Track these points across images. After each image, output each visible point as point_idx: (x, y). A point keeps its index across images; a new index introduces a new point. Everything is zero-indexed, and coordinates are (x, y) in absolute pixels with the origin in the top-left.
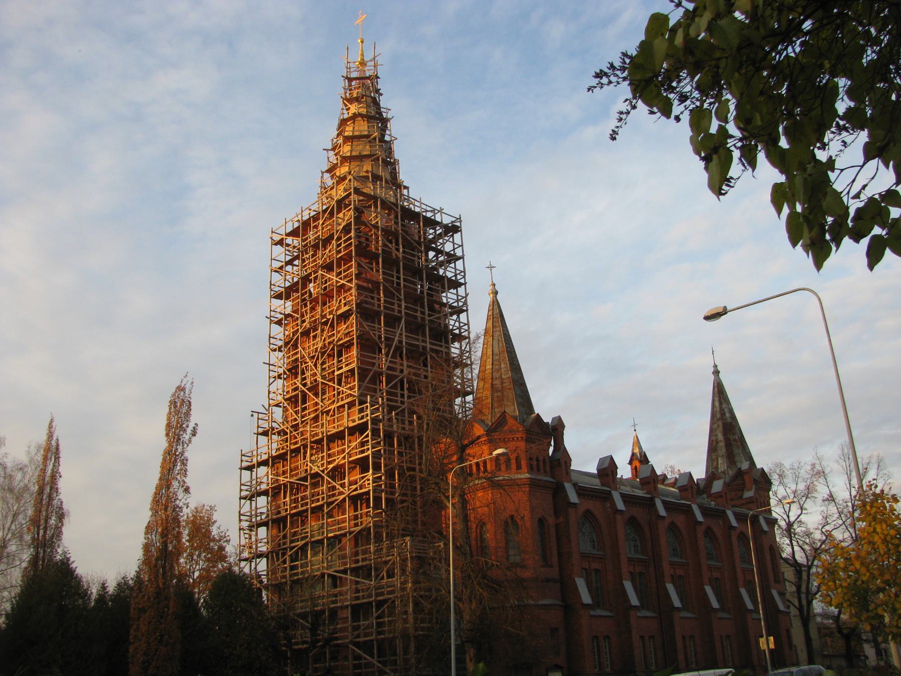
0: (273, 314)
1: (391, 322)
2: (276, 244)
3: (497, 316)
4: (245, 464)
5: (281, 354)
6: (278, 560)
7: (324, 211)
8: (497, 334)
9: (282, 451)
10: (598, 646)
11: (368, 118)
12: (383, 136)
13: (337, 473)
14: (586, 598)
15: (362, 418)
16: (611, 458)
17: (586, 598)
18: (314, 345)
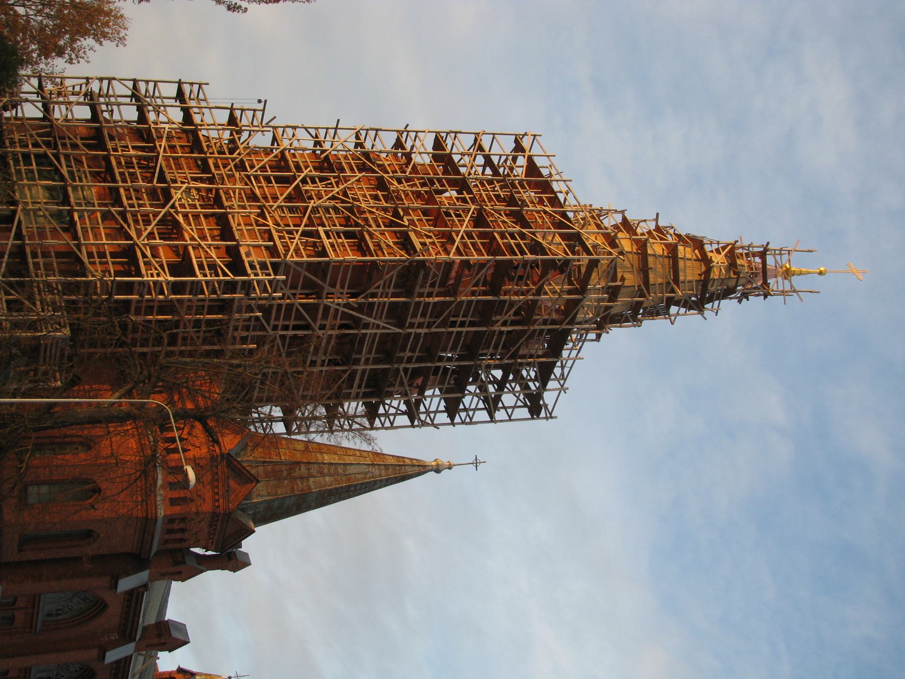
0: (413, 135)
1: (397, 314)
2: (516, 141)
3: (402, 471)
4: (186, 88)
5: (351, 146)
7: (564, 215)
8: (376, 471)
9: (204, 145)
11: (705, 281)
12: (677, 304)
13: (171, 228)
15: (252, 267)
16: (185, 642)
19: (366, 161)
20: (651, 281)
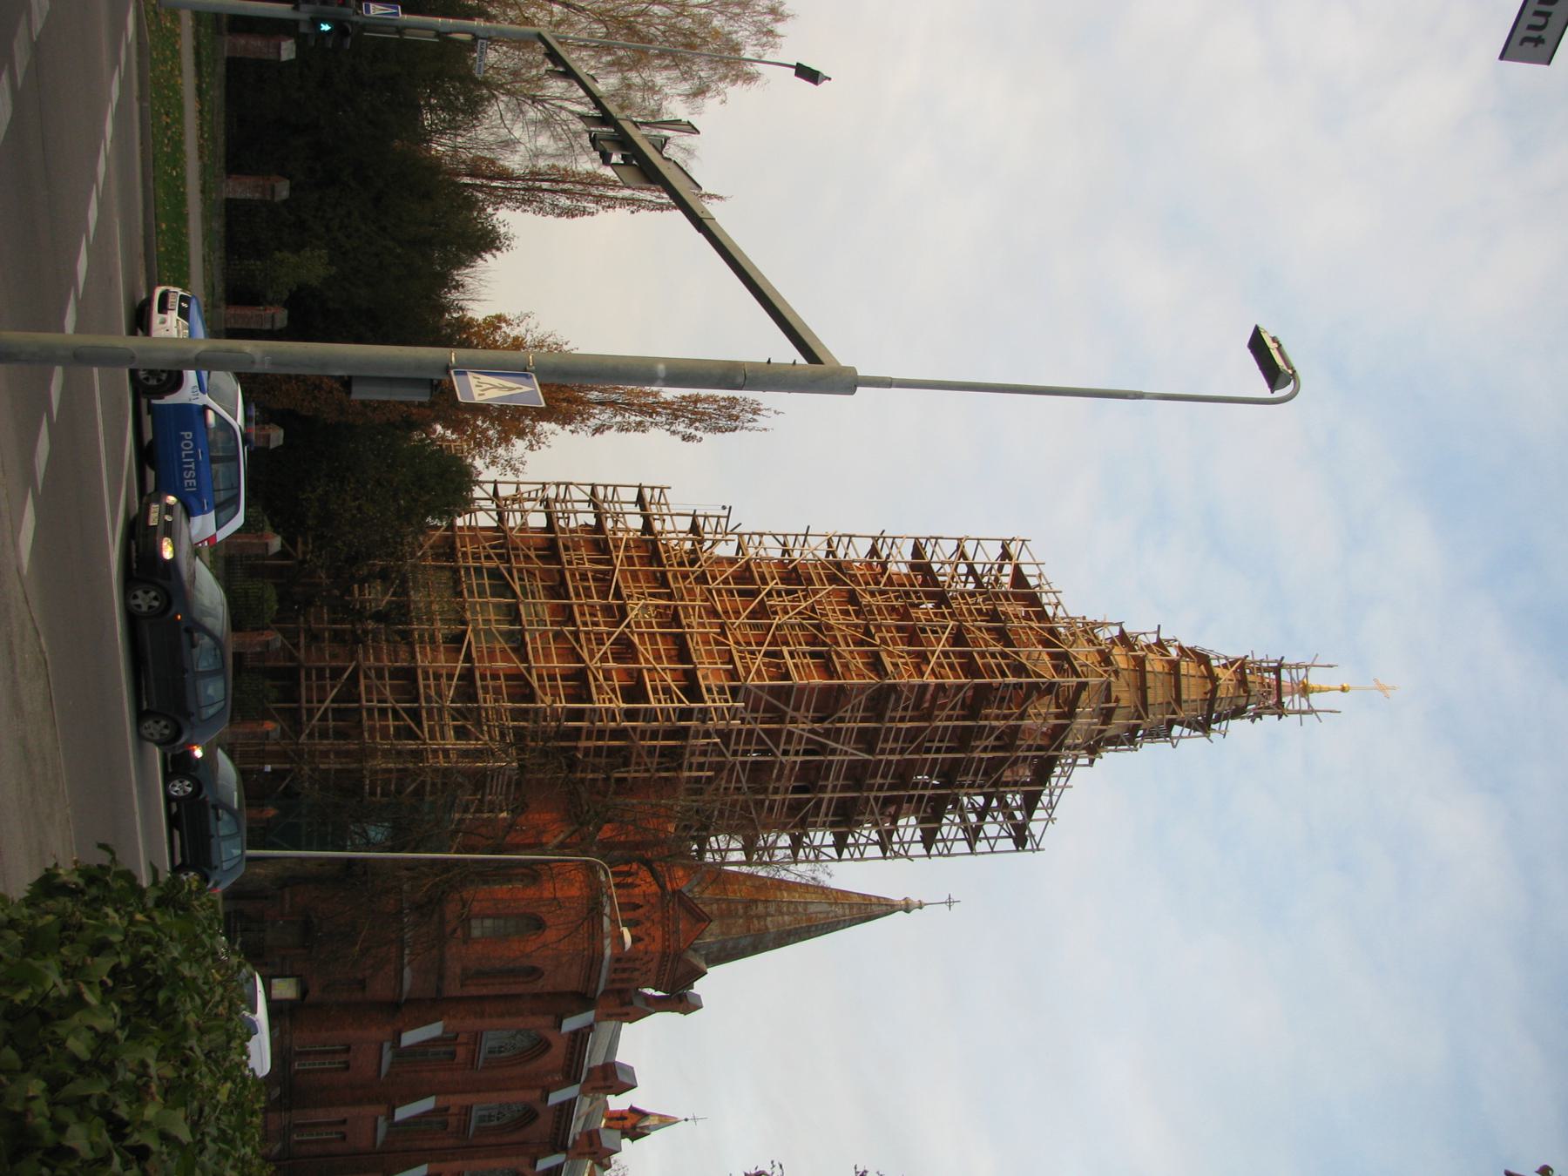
0: (889, 541)
1: (867, 740)
2: (1003, 547)
3: (867, 909)
4: (647, 493)
5: (822, 555)
6: (493, 547)
7: (1052, 631)
9: (664, 556)
10: (334, 1052)
11: (1211, 699)
12: (1181, 724)
13: (625, 651)
14: (410, 1038)
15: (709, 690)
16: (633, 1087)
17: (410, 1038)
18: (834, 611)
19: (837, 571)
20: (1150, 700)
